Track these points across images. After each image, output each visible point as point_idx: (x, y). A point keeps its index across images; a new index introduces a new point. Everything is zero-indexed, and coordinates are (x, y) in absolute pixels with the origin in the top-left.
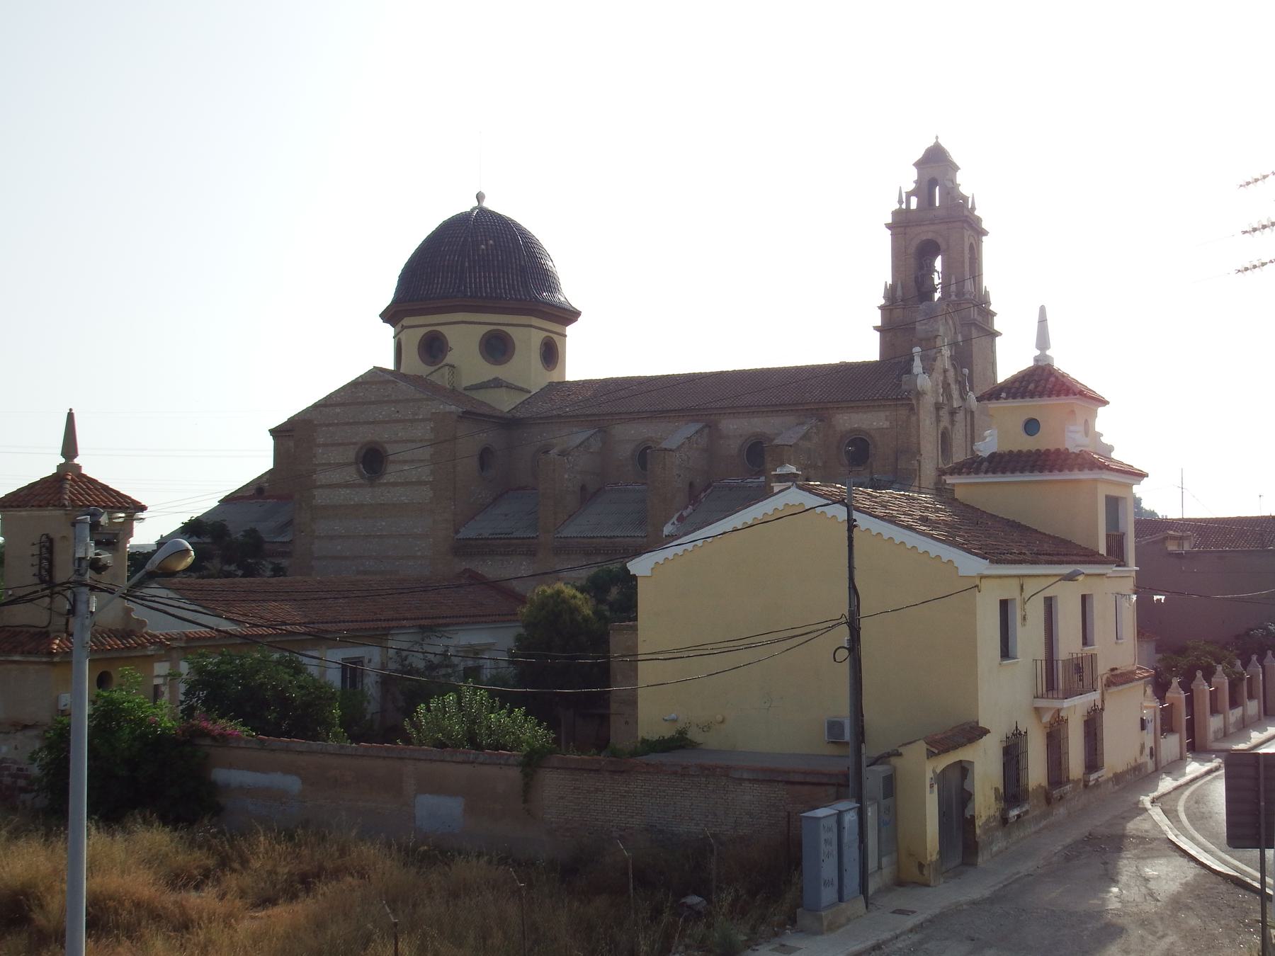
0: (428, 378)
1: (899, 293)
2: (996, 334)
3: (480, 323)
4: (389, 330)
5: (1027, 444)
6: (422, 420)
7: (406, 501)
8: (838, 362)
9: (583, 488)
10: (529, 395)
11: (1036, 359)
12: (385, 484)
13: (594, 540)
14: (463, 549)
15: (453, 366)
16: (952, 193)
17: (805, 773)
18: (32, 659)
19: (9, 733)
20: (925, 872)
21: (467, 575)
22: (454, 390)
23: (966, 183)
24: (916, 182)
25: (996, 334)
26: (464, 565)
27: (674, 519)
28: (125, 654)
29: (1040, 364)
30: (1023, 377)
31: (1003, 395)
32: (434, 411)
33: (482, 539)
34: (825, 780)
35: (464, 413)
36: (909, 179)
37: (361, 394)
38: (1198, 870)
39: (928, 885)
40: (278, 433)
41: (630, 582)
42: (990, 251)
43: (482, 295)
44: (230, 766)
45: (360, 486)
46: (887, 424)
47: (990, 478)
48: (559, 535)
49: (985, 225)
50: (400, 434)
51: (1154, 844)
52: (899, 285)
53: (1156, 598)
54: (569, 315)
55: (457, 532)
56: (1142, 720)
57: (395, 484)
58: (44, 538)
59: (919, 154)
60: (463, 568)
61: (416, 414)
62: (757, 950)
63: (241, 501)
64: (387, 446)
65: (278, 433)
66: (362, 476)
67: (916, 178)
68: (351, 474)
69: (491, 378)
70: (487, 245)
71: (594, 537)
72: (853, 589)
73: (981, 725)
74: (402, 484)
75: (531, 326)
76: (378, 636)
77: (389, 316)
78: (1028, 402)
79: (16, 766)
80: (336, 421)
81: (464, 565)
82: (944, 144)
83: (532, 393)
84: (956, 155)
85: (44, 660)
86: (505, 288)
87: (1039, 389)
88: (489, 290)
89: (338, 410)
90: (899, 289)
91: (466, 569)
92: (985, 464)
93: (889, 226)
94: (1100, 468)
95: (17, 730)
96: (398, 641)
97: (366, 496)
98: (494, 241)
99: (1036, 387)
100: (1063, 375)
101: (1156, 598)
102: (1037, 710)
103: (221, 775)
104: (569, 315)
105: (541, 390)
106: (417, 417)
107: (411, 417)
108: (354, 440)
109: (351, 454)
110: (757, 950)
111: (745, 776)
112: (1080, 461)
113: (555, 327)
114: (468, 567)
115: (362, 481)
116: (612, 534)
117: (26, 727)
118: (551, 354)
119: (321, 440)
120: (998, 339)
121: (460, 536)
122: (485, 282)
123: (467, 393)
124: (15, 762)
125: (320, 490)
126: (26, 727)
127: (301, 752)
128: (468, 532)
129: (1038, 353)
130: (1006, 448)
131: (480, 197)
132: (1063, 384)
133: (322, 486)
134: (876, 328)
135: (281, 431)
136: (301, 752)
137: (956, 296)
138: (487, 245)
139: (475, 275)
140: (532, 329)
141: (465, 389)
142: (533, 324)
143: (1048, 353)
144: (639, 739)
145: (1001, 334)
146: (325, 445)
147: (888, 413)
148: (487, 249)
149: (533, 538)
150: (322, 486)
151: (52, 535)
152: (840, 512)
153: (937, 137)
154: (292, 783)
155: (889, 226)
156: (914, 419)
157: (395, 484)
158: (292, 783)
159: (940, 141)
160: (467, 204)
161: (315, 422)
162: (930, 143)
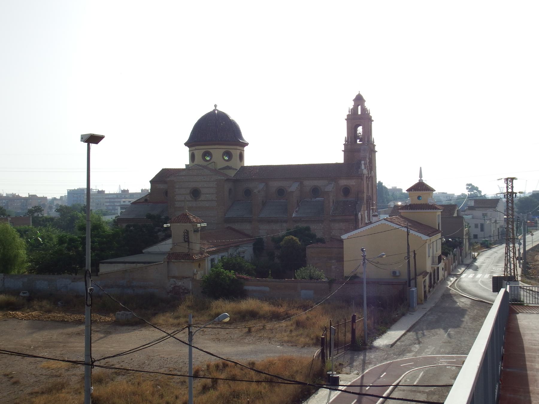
0: (207, 166)
3: (223, 149)
4: (187, 149)
7: (208, 206)
8: (335, 163)
10: (237, 171)
11: (419, 180)
14: (228, 220)
15: (214, 162)
16: (364, 110)
19: (181, 279)
22: (215, 169)
27: (295, 212)
28: (201, 259)
31: (413, 190)
32: (216, 178)
35: (227, 179)
36: (351, 105)
38: (470, 300)
39: (423, 304)
40: (151, 182)
41: (342, 241)
42: (374, 125)
43: (223, 140)
46: (354, 184)
49: (373, 119)
51: (458, 296)
52: (350, 137)
53: (449, 239)
55: (225, 215)
56: (443, 268)
58: (185, 231)
59: (354, 97)
62: (413, 314)
65: (151, 182)
67: (353, 105)
68: (189, 198)
72: (408, 244)
76: (226, 250)
77: (186, 144)
78: (419, 192)
82: (362, 94)
83: (238, 170)
84: (365, 97)
85: (191, 261)
86: (230, 138)
88: (225, 138)
89: (183, 177)
90: (350, 139)
91: (228, 227)
92: (409, 207)
93: (346, 119)
95: (184, 279)
96: (231, 251)
98: (225, 122)
99: (421, 188)
101: (449, 239)
106: (211, 180)
111: (383, 283)
113: (240, 148)
114: (229, 226)
116: (277, 216)
117: (186, 278)
118: (241, 157)
119: (177, 187)
120: (376, 153)
121: (226, 217)
122: (224, 136)
123: (219, 171)
126: (186, 278)
130: (413, 203)
131: (215, 106)
132: (427, 188)
134: (343, 151)
141: (219, 169)
143: (422, 179)
145: (377, 152)
150: (178, 201)
151: (188, 230)
152: (406, 230)
153: (359, 92)
154: (267, 289)
155: (346, 119)
157: (203, 201)
158: (267, 289)
160: (210, 109)
161: (175, 181)
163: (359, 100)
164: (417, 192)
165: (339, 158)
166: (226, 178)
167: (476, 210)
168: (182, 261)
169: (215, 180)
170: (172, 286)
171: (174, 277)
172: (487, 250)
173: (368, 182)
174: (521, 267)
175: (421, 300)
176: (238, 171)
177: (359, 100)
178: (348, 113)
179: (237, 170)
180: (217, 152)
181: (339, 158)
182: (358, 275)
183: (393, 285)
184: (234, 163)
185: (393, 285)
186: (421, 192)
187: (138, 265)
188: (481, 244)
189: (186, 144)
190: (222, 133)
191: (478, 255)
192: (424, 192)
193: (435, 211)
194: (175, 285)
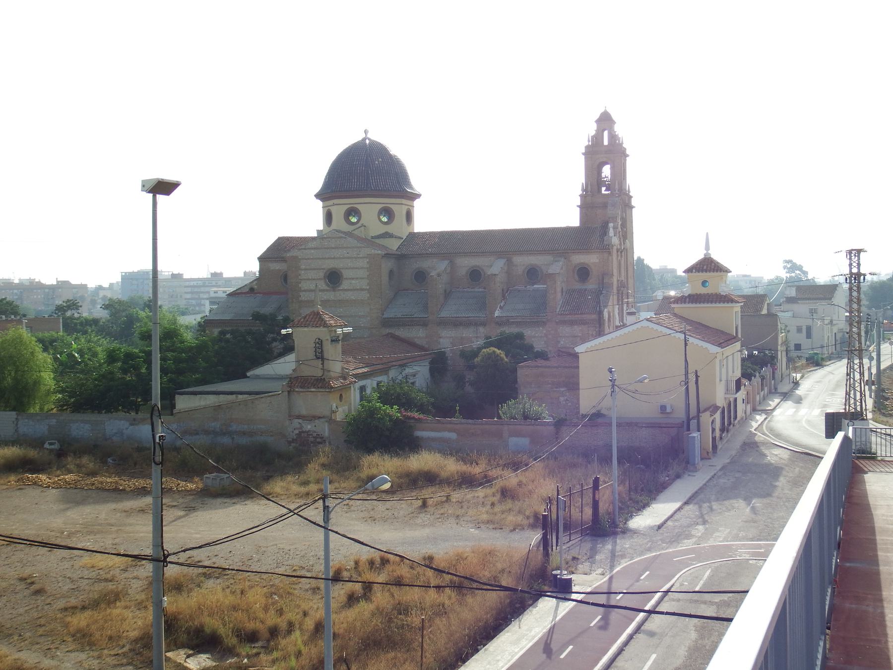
1: (589, 188)
2: (633, 207)
4: (319, 204)
5: (703, 291)
6: (361, 258)
7: (354, 299)
9: (445, 291)
10: (402, 241)
12: (341, 290)
13: (458, 319)
14: (387, 323)
16: (613, 137)
17: (666, 424)
18: (321, 390)
20: (709, 454)
21: (390, 336)
23: (619, 129)
24: (596, 131)
25: (633, 207)
26: (388, 331)
29: (707, 257)
30: (701, 262)
31: (694, 271)
32: (368, 253)
33: (398, 318)
34: (673, 426)
35: (385, 254)
37: (326, 243)
38: (789, 452)
41: (576, 356)
44: (423, 430)
45: (327, 290)
46: (597, 261)
47: (690, 305)
48: (440, 316)
49: (627, 152)
50: (349, 265)
54: (415, 196)
55: (383, 314)
57: (346, 290)
58: (317, 340)
59: (597, 116)
60: (387, 332)
61: (359, 255)
63: (237, 296)
64: (343, 271)
66: (328, 285)
67: (596, 129)
68: (322, 285)
69: (384, 232)
70: (378, 161)
71: (458, 317)
72: (686, 361)
73: (717, 405)
74: (351, 290)
75: (402, 204)
76: (385, 371)
77: (319, 196)
78: (704, 274)
79: (315, 434)
80: (312, 257)
81: (388, 331)
83: (404, 239)
84: (614, 117)
86: (390, 185)
87: (709, 268)
89: (313, 251)
92: (688, 299)
93: (583, 154)
94: (736, 303)
96: (393, 373)
97: (331, 296)
98: (382, 159)
99: (707, 267)
100: (718, 263)
101: (754, 352)
102: (725, 398)
103: (418, 433)
104: (415, 196)
105: (407, 236)
107: (355, 256)
108: (322, 267)
109: (321, 274)
110: (695, 476)
111: (644, 425)
112: (726, 299)
115: (328, 288)
117: (320, 418)
119: (303, 267)
121: (385, 316)
124: (315, 432)
125: (304, 293)
126: (320, 418)
127: (457, 424)
128: (390, 314)
129: (705, 252)
130: (694, 292)
131: (366, 132)
133: (305, 291)
134: (578, 206)
135: (261, 259)
136: (457, 424)
137: (618, 191)
138: (378, 161)
139: (374, 178)
140: (403, 206)
141: (372, 237)
142: (403, 203)
143: (709, 252)
144: (581, 414)
146: (306, 269)
147: (598, 256)
148: (379, 164)
149: (426, 317)
150: (305, 291)
152: (682, 336)
154: (453, 436)
155: (583, 154)
156: (610, 258)
157: (346, 290)
158: (453, 436)
159: (607, 109)
161: (300, 258)
162: (603, 110)
163: (605, 121)
164: (701, 274)
165: (571, 218)
166: (383, 253)
167: (798, 303)
168: (312, 390)
169: (366, 256)
170: (297, 432)
171: (299, 417)
172: (817, 370)
173: (619, 258)
174: (873, 397)
175: (708, 453)
176: (404, 241)
177: (605, 121)
178: (587, 144)
179: (403, 239)
180: (369, 209)
181: (571, 218)
182: (604, 412)
183: (661, 427)
184: (398, 228)
185: (661, 427)
186: (708, 274)
187: (240, 396)
188: (807, 359)
189: (319, 196)
190: (377, 177)
191: (802, 377)
192: (712, 274)
193: (730, 305)
194: (300, 430)
